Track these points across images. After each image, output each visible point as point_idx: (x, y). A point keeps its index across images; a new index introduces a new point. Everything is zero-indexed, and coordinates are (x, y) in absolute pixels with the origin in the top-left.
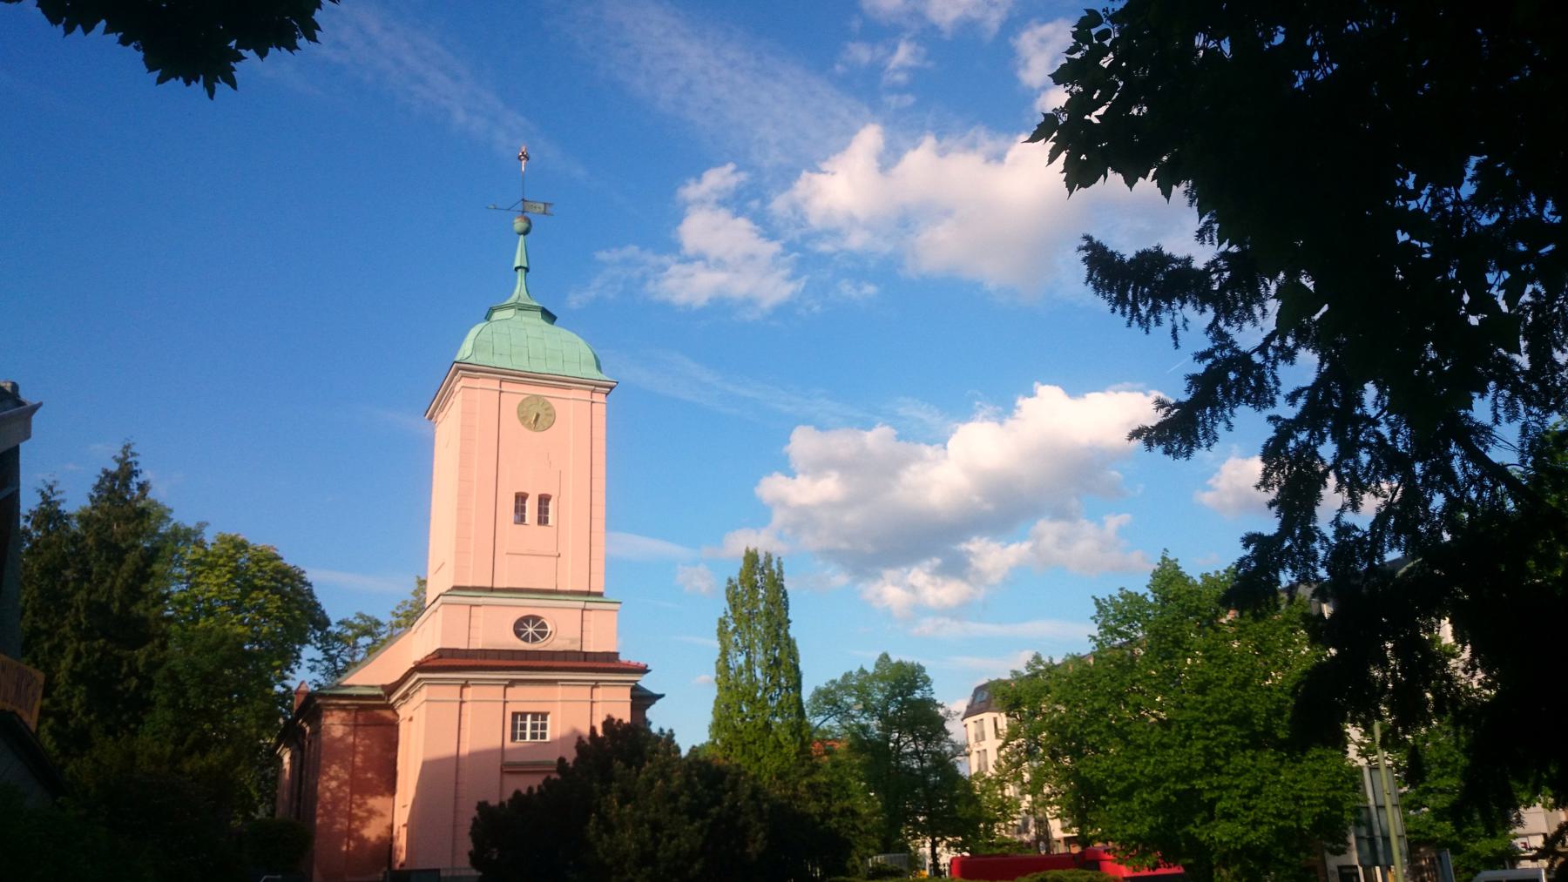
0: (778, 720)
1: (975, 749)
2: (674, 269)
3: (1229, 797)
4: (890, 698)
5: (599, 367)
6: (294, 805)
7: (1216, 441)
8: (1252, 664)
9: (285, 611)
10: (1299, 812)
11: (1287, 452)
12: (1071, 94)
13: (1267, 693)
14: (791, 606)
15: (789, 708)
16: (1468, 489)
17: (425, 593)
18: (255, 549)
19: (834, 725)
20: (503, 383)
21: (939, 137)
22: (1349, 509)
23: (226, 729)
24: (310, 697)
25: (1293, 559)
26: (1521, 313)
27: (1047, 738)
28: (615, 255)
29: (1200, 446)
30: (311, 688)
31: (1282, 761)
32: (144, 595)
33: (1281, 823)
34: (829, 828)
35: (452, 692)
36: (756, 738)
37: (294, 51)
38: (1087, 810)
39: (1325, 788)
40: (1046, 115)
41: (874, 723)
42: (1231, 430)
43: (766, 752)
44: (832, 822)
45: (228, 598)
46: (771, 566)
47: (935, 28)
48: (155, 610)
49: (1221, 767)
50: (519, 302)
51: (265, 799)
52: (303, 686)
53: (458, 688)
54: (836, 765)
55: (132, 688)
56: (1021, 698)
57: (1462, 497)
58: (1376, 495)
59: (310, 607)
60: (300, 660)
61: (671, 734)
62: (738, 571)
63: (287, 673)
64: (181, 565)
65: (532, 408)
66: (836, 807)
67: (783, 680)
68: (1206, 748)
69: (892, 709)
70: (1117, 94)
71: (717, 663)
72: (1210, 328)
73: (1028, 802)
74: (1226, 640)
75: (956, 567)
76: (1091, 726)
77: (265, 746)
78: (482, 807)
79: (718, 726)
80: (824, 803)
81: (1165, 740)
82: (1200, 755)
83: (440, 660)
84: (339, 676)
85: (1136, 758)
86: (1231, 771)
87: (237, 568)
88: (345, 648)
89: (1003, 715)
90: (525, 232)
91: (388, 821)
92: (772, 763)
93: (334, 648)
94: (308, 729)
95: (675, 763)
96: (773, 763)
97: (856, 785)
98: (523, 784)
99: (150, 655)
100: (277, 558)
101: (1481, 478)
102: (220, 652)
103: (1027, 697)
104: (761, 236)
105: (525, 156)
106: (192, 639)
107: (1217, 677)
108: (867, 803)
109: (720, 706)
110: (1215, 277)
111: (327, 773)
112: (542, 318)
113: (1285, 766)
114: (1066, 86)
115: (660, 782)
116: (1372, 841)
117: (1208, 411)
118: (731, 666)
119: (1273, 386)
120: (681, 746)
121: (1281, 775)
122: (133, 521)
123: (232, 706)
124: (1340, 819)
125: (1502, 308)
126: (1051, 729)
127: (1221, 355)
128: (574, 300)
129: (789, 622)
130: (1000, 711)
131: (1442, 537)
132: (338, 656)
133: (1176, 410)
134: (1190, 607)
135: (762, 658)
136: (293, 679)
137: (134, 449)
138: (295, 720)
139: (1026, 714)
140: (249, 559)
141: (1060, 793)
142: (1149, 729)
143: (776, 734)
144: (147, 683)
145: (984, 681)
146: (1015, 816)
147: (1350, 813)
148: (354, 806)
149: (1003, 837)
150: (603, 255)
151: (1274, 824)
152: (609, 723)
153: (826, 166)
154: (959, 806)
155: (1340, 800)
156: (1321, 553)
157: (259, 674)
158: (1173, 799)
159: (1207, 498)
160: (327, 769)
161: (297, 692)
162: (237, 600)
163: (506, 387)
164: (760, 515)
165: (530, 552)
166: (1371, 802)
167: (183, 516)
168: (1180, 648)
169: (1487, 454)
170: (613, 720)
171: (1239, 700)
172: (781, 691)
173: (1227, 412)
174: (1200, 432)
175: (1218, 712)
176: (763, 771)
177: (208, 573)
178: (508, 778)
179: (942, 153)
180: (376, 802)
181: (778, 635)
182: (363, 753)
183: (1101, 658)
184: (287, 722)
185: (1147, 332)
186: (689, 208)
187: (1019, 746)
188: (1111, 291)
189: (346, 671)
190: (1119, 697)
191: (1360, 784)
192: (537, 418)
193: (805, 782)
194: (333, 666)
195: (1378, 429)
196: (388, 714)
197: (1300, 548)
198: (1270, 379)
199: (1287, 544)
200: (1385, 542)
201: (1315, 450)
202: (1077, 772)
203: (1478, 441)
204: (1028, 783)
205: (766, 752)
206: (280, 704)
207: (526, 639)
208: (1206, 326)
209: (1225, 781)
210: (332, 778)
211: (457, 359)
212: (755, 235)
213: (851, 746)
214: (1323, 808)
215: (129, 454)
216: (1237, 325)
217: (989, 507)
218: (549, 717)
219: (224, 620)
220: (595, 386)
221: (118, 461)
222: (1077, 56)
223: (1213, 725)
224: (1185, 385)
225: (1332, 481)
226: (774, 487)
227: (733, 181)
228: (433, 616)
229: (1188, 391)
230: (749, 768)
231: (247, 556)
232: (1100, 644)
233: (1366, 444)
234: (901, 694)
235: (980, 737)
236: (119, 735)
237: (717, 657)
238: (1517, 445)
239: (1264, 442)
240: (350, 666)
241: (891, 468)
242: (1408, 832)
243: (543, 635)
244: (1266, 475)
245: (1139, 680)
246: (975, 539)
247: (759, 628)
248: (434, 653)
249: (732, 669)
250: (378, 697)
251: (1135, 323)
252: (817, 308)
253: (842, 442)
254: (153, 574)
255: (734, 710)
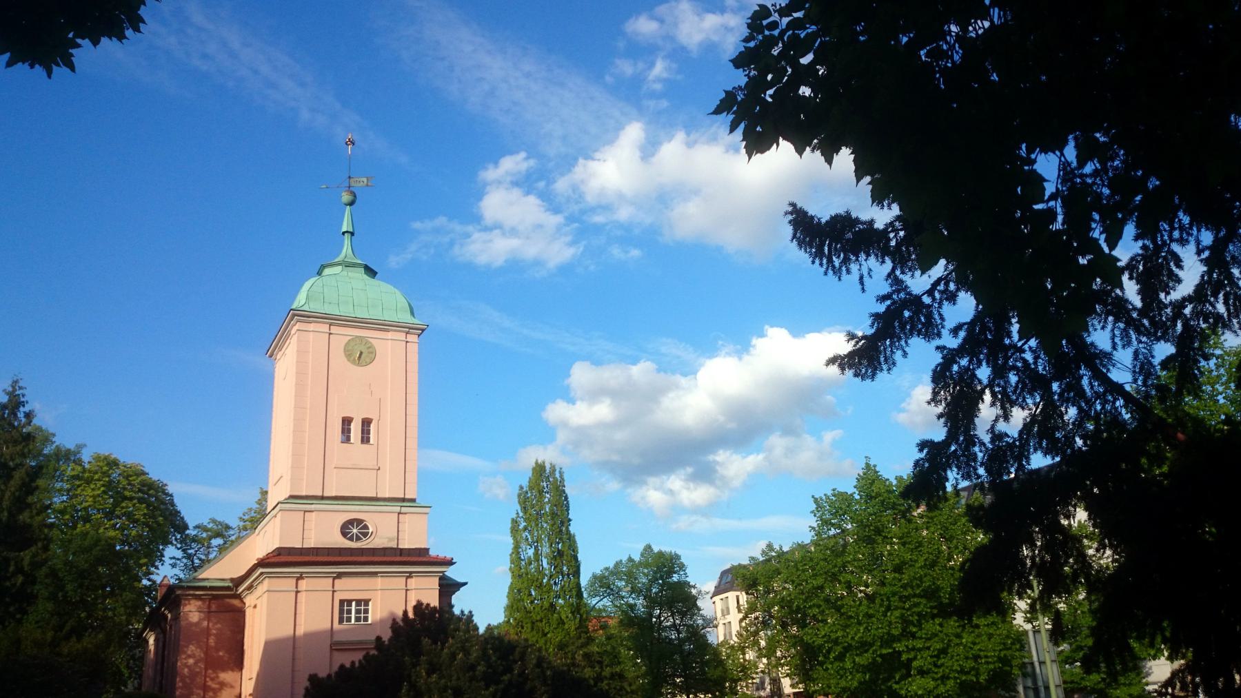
0: (561, 601)
1: (722, 622)
2: (476, 235)
3: (922, 658)
4: (653, 581)
5: (412, 313)
6: (158, 681)
7: (894, 366)
8: (938, 548)
9: (150, 518)
10: (978, 669)
11: (952, 375)
12: (749, 77)
13: (950, 571)
14: (571, 508)
15: (570, 591)
16: (1095, 402)
17: (266, 502)
18: (125, 466)
19: (608, 604)
20: (332, 327)
21: (688, 134)
22: (1001, 420)
23: (100, 617)
24: (171, 589)
25: (958, 461)
26: (1134, 263)
27: (778, 611)
28: (429, 224)
29: (882, 370)
30: (172, 581)
31: (964, 627)
32: (29, 506)
33: (964, 678)
34: (601, 690)
35: (289, 584)
36: (543, 616)
37: (124, 41)
38: (811, 669)
39: (998, 648)
40: (726, 92)
41: (640, 602)
42: (906, 357)
43: (552, 628)
44: (603, 684)
45: (101, 507)
46: (555, 475)
47: (683, 49)
48: (40, 518)
49: (915, 633)
50: (346, 260)
51: (134, 675)
52: (166, 579)
53: (294, 581)
54: (609, 638)
55: (18, 584)
56: (757, 579)
57: (1090, 409)
58: (1023, 408)
59: (171, 514)
60: (163, 559)
61: (471, 614)
62: (528, 479)
63: (153, 569)
64: (62, 481)
65: (356, 347)
66: (607, 672)
67: (565, 568)
68: (902, 616)
69: (654, 590)
70: (786, 78)
71: (511, 555)
72: (889, 276)
73: (764, 664)
74: (917, 529)
75: (705, 474)
76: (811, 601)
77: (133, 631)
78: (313, 678)
79: (512, 608)
80: (597, 669)
81: (871, 611)
82: (898, 622)
83: (279, 557)
84: (196, 571)
85: (847, 626)
86: (924, 636)
87: (110, 482)
88: (201, 548)
89: (744, 593)
90: (351, 204)
91: (237, 692)
92: (556, 637)
93: (191, 548)
94: (169, 616)
95: (474, 639)
96: (557, 637)
97: (626, 653)
98: (347, 659)
99: (34, 556)
100: (144, 473)
101: (1104, 394)
102: (94, 552)
103: (762, 578)
104: (548, 210)
105: (351, 142)
106: (70, 541)
107: (910, 559)
108: (634, 667)
109: (513, 591)
110: (892, 235)
111: (185, 653)
112: (365, 273)
113: (966, 630)
114: (744, 71)
115: (460, 655)
116: (1036, 690)
117: (888, 343)
118: (522, 557)
119: (939, 321)
120: (479, 625)
121: (963, 638)
122: (21, 443)
123: (105, 597)
124: (1010, 673)
125: (1105, 249)
126: (781, 604)
127: (898, 297)
128: (394, 261)
129: (570, 520)
130: (741, 590)
131: (1075, 442)
132: (195, 555)
133: (863, 341)
134: (888, 503)
135: (548, 550)
136: (158, 574)
137: (21, 384)
138: (158, 608)
139: (762, 592)
140: (119, 475)
141: (789, 656)
142: (858, 603)
143: (559, 613)
144: (31, 579)
145: (728, 566)
146: (754, 676)
147: (1017, 668)
148: (208, 679)
149: (745, 693)
150: (417, 225)
151: (958, 678)
152: (418, 607)
153: (597, 155)
154: (709, 669)
155: (1010, 658)
156: (980, 455)
157: (127, 570)
158: (879, 659)
159: (902, 417)
160: (185, 649)
161: (160, 585)
162: (110, 508)
163: (334, 329)
164: (547, 434)
165: (354, 467)
166: (1035, 659)
167: (65, 439)
168: (880, 535)
169: (1109, 374)
170: (422, 604)
171: (928, 577)
172: (563, 577)
173: (903, 343)
174: (882, 359)
175: (912, 588)
176: (549, 644)
177: (85, 487)
178: (336, 654)
179: (690, 145)
180: (226, 676)
181: (561, 531)
182: (215, 635)
183: (819, 545)
184: (153, 611)
185: (840, 279)
186: (488, 188)
187: (756, 618)
188: (811, 247)
189: (202, 567)
190: (834, 578)
191: (1026, 644)
192: (361, 356)
193: (581, 652)
194: (191, 563)
195: (1023, 355)
196: (236, 602)
197: (964, 452)
198: (936, 316)
199: (953, 448)
200: (1030, 446)
201: (974, 372)
202: (802, 640)
203: (1101, 364)
204: (764, 648)
205: (552, 628)
206: (147, 595)
207: (351, 539)
208: (886, 274)
209: (919, 644)
210: (189, 656)
211: (294, 307)
212: (542, 209)
213: (621, 621)
214: (997, 665)
215: (17, 388)
216: (910, 274)
217: (732, 426)
218: (370, 603)
219: (99, 524)
220: (409, 329)
221: (8, 393)
222: (752, 44)
223: (908, 598)
224: (869, 322)
225: (988, 397)
226: (557, 411)
227: (524, 166)
228: (272, 520)
229: (872, 326)
230: (537, 641)
231: (118, 472)
232: (819, 534)
233: (1014, 368)
234: (661, 578)
235: (726, 612)
236: (7, 624)
237: (511, 551)
238: (1130, 367)
239: (933, 367)
240: (205, 563)
241: (653, 395)
242: (1065, 682)
243: (365, 535)
244: (935, 394)
245: (849, 562)
246: (721, 452)
247: (545, 525)
248: (273, 551)
249: (522, 560)
250: (228, 588)
251: (830, 272)
252: (592, 268)
253: (612, 375)
254: (37, 488)
255: (525, 594)
